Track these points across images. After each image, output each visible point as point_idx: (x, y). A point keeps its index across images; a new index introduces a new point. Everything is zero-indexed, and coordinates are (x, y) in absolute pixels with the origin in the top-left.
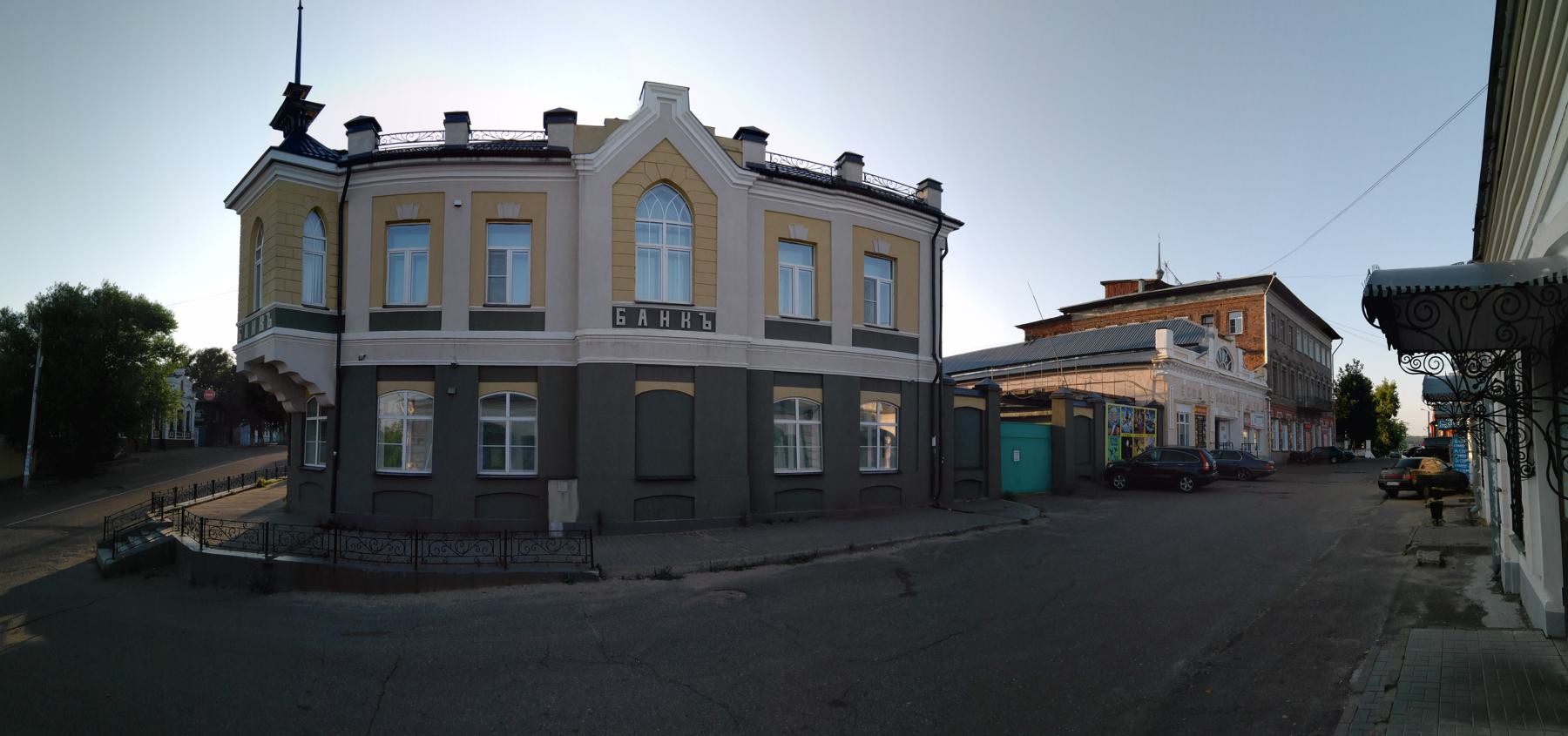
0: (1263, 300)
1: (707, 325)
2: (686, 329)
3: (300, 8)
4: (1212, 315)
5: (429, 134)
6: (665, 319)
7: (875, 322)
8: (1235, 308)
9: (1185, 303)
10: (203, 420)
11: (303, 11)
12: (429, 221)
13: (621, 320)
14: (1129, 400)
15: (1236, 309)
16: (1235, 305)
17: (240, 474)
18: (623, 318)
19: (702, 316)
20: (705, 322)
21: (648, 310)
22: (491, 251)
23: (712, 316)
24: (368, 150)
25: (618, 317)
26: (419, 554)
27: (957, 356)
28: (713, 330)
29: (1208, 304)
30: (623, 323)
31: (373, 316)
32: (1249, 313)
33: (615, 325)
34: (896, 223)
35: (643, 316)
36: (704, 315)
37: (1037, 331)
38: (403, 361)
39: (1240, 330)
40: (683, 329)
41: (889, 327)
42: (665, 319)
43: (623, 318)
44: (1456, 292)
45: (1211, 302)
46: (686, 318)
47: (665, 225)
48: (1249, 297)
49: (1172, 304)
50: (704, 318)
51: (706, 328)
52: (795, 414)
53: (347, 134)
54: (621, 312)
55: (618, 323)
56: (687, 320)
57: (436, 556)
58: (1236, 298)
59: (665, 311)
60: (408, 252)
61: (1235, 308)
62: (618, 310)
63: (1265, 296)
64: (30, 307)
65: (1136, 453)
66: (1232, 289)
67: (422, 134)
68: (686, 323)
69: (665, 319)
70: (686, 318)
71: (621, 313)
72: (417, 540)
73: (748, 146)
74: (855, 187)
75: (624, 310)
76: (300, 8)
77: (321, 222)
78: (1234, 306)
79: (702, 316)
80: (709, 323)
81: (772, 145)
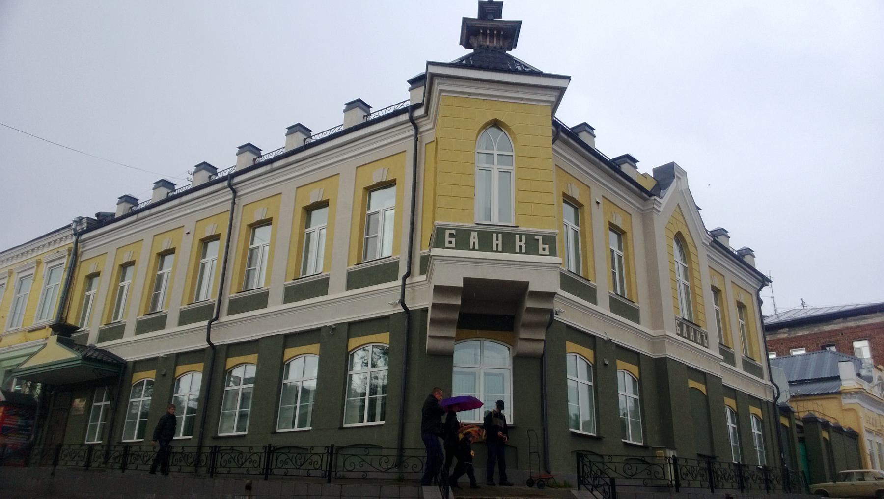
1: (544, 249)
6: (497, 242)
9: (800, 333)
10: (736, 253)
12: (339, 174)
17: (673, 308)
18: (453, 240)
19: (538, 240)
20: (541, 246)
21: (480, 233)
30: (453, 245)
34: (192, 204)
35: (474, 239)
36: (540, 238)
40: (517, 253)
42: (497, 242)
43: (453, 240)
46: (520, 241)
47: (495, 157)
49: (785, 336)
50: (541, 242)
52: (383, 394)
53: (287, 135)
54: (451, 235)
56: (522, 244)
59: (520, 235)
64: (656, 171)
68: (520, 247)
69: (497, 242)
70: (520, 241)
71: (451, 235)
74: (286, 155)
75: (454, 232)
79: (538, 240)
80: (547, 247)
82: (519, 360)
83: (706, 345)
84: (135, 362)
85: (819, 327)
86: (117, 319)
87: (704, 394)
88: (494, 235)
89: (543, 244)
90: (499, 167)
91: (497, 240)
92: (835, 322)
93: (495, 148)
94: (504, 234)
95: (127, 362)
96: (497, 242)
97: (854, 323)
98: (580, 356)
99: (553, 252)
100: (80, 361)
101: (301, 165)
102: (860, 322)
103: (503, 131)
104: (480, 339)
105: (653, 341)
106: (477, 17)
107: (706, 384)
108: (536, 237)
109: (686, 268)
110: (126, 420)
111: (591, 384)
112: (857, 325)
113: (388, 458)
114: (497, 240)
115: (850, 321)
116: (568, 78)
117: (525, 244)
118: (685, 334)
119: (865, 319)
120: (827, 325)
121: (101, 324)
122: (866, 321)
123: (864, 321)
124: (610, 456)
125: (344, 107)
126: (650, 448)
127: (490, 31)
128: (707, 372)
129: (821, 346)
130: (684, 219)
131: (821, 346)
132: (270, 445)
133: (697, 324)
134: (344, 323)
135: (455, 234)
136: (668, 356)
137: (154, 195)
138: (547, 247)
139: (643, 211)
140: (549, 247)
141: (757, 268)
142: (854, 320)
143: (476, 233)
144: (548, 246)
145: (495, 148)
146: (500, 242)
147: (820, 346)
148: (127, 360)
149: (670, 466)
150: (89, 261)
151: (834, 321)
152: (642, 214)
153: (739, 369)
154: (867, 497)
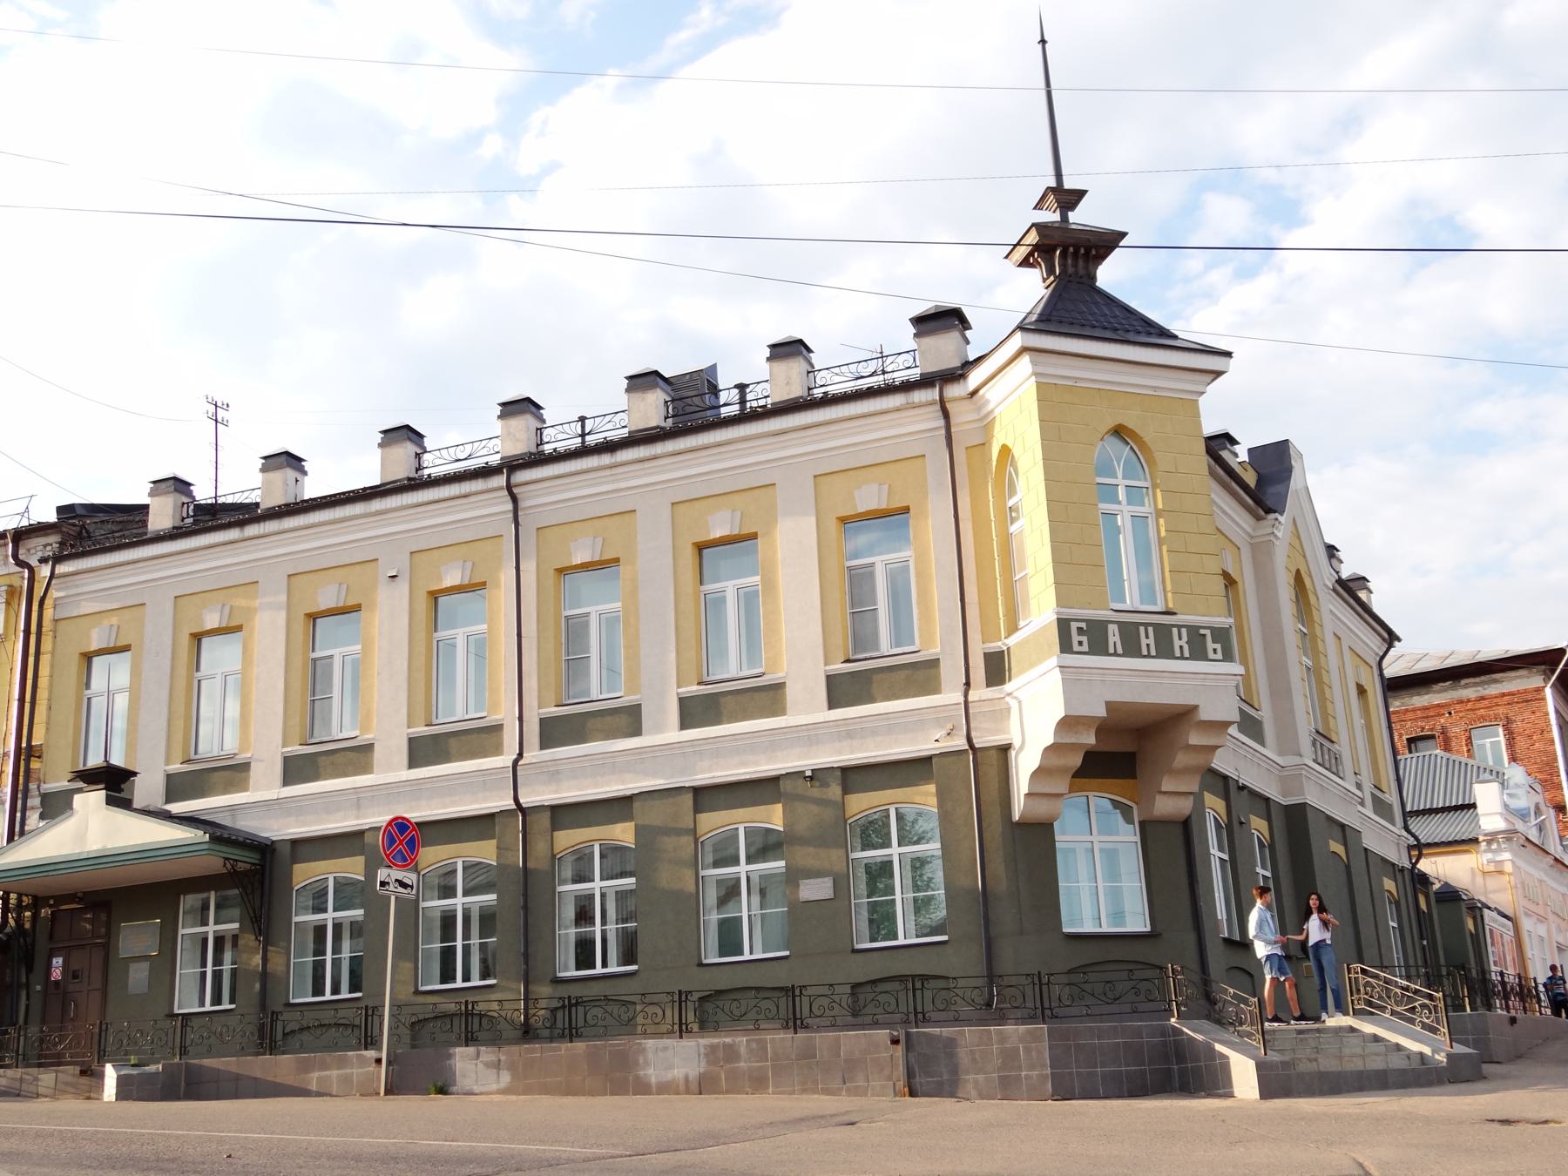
0: (1544, 699)
3: (1043, 42)
4: (1432, 737)
5: (484, 443)
8: (1483, 718)
11: (1047, 46)
14: (70, 1089)
15: (1487, 722)
16: (1482, 712)
18: (1084, 639)
19: (1204, 635)
20: (1210, 645)
22: (568, 618)
24: (653, 424)
25: (1075, 638)
26: (1046, 1005)
29: (1419, 713)
31: (289, 762)
32: (1518, 726)
36: (1207, 632)
38: (303, 829)
43: (1084, 639)
45: (1425, 708)
48: (1509, 694)
51: (1215, 657)
54: (1080, 630)
56: (1183, 642)
57: (1068, 1006)
58: (1483, 698)
60: (461, 635)
61: (1483, 718)
62: (1074, 626)
66: (1472, 680)
67: (476, 444)
69: (1147, 641)
70: (1180, 639)
72: (914, 990)
75: (1083, 625)
76: (1043, 42)
78: (1481, 716)
80: (1218, 646)
82: (1149, 830)
83: (1342, 775)
84: (295, 843)
85: (1403, 698)
86: (1419, 883)
87: (1343, 860)
88: (1142, 629)
89: (1213, 642)
90: (1131, 508)
91: (1147, 637)
92: (1436, 687)
93: (1120, 475)
94: (1156, 626)
95: (273, 842)
96: (1148, 641)
97: (1476, 691)
98: (1215, 814)
99: (1228, 657)
100: (206, 847)
101: (682, 461)
102: (1485, 689)
103: (1128, 444)
104: (1086, 793)
105: (1289, 779)
106: (1059, 220)
107: (1345, 844)
108: (1202, 631)
109: (1305, 634)
110: (292, 961)
111: (1226, 857)
112: (1480, 694)
113: (877, 1000)
114: (1147, 637)
115: (1466, 686)
116: (1228, 354)
117: (1187, 643)
118: (1320, 760)
119: (1496, 681)
120: (1419, 694)
121: (168, 762)
122: (1498, 685)
123: (1493, 686)
124: (831, 985)
125: (767, 353)
126: (1294, 958)
127: (1085, 249)
128: (1347, 823)
129: (1407, 739)
130: (1301, 542)
131: (1407, 739)
132: (569, 997)
133: (1326, 735)
134: (833, 767)
135: (1085, 629)
136: (1308, 802)
137: (265, 488)
138: (1218, 646)
139: (1252, 537)
140: (1222, 647)
141: (1376, 610)
142: (1476, 685)
143: (1116, 626)
144: (1219, 645)
145: (1120, 475)
146: (1151, 641)
147: (1404, 738)
148: (274, 839)
149: (914, 995)
150: (76, 620)
151: (1434, 686)
152: (1251, 544)
153: (1369, 812)
154: (112, 1162)
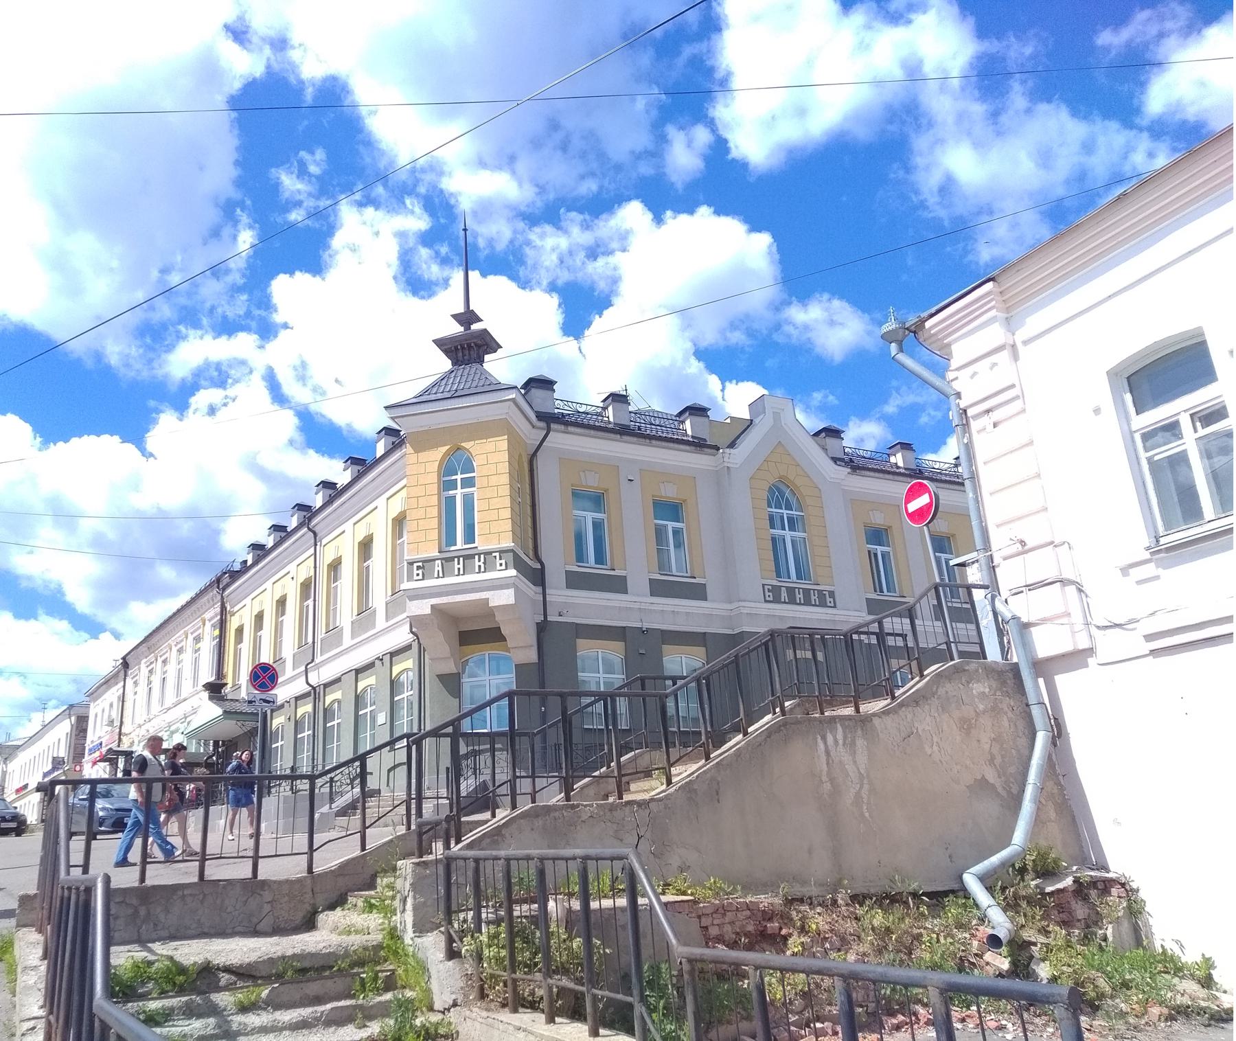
2: (815, 605)
7: (670, 570)
13: (418, 575)
18: (771, 594)
20: (828, 599)
23: (832, 594)
25: (767, 594)
27: (1059, 699)
28: (835, 607)
33: (766, 601)
37: (279, 529)
39: (909, 720)
40: (813, 605)
41: (686, 575)
44: (361, 751)
50: (827, 595)
55: (768, 599)
62: (766, 587)
63: (599, 993)
65: (966, 261)
73: (537, 394)
77: (992, 563)
80: (832, 600)
81: (559, 391)
